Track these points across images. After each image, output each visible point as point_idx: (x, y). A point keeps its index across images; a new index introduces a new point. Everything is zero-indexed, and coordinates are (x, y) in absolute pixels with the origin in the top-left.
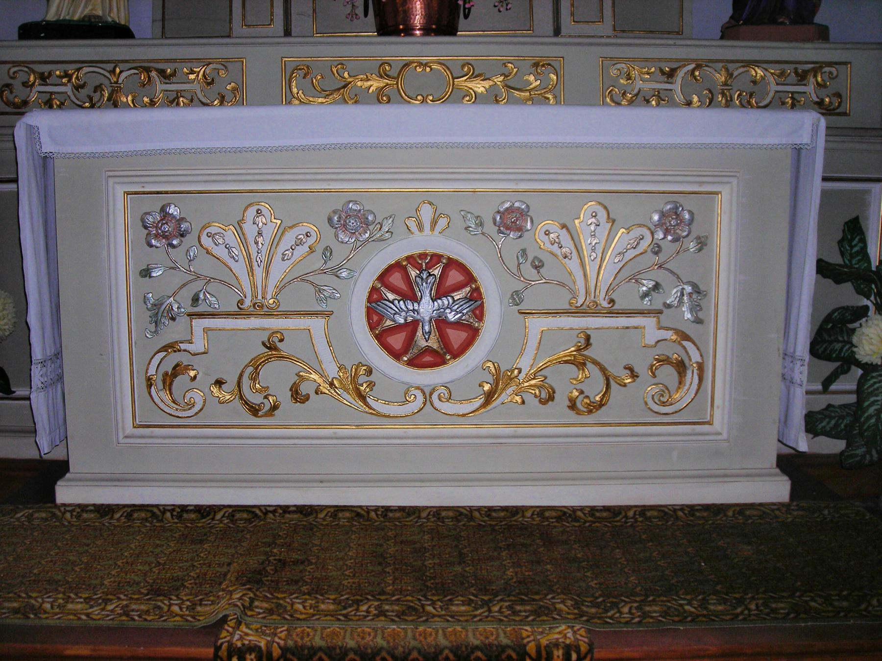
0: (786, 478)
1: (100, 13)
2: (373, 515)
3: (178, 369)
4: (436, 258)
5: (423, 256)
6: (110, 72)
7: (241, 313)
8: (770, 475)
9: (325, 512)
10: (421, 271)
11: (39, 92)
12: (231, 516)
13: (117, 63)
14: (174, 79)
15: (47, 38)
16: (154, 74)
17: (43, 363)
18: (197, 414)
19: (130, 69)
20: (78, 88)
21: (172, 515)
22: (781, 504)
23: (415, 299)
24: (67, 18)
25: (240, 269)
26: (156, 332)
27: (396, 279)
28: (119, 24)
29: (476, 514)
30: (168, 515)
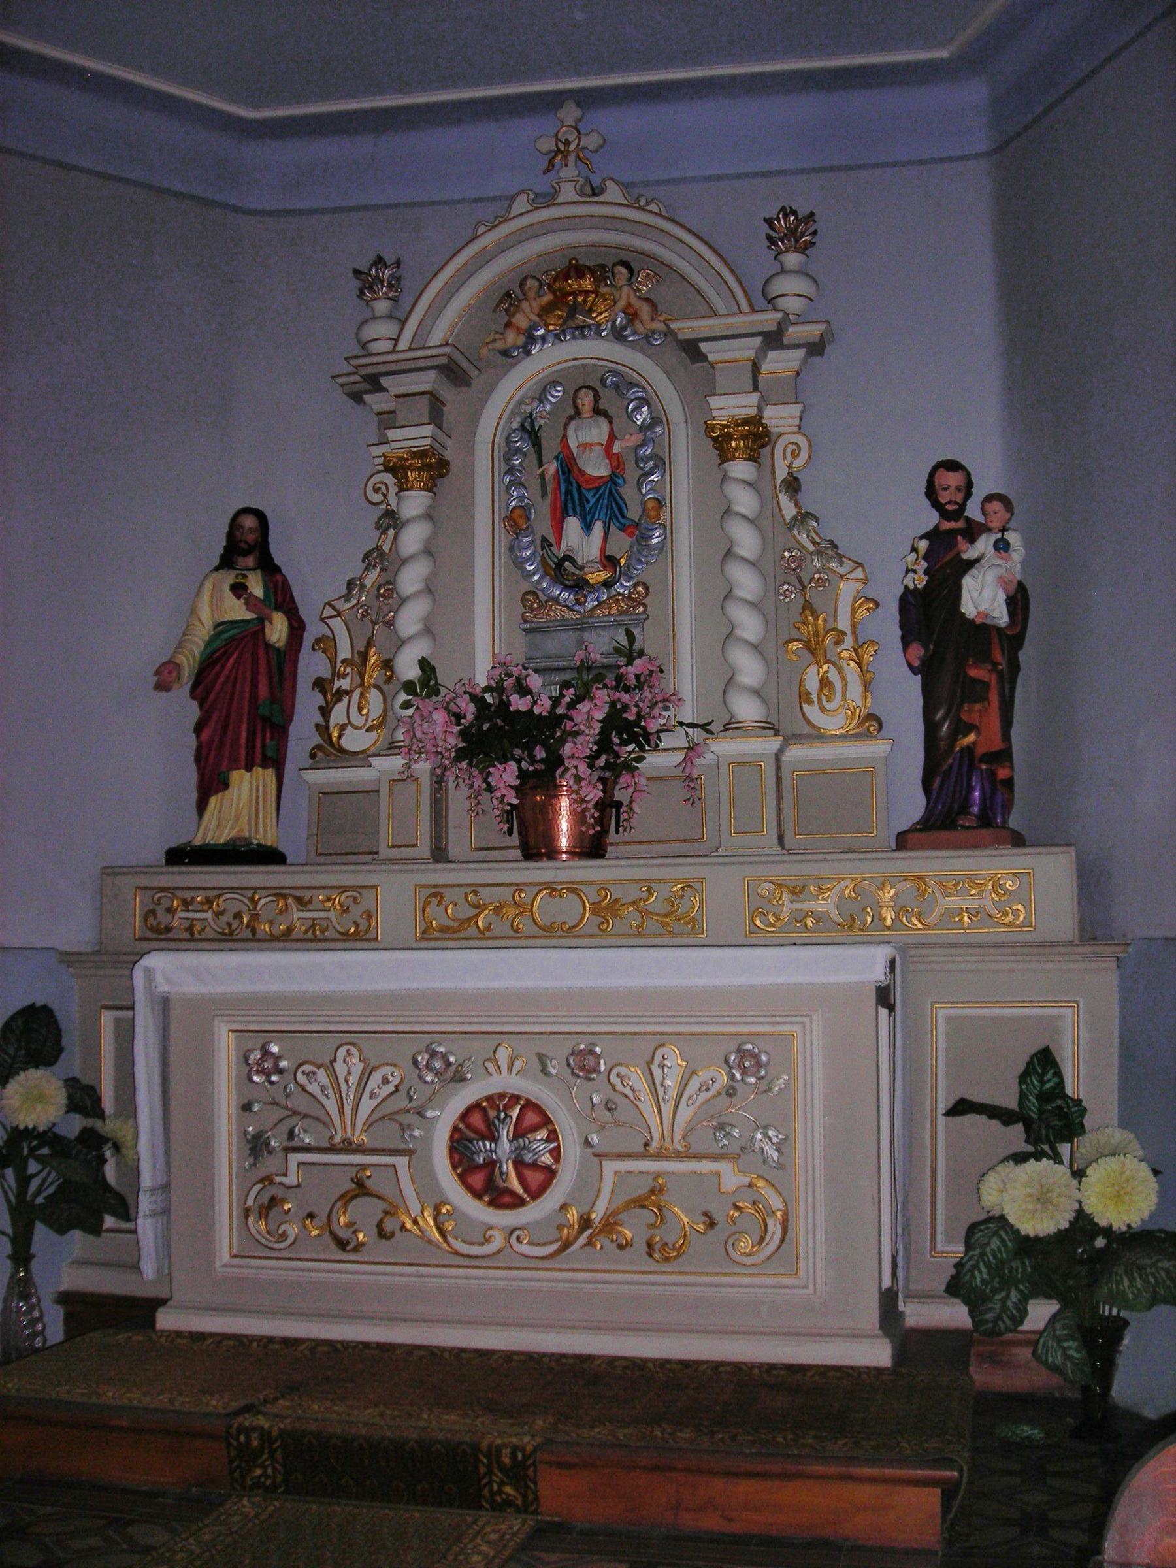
0: (887, 1340)
1: (247, 834)
2: (446, 1355)
3: (274, 1202)
4: (515, 1099)
5: (502, 1096)
6: (248, 898)
7: (332, 1149)
8: (872, 1337)
9: (813, 1371)
10: (499, 1111)
11: (181, 918)
12: (313, 1350)
13: (256, 889)
14: (310, 907)
15: (191, 863)
16: (290, 901)
17: (153, 1191)
18: (290, 1246)
19: (268, 896)
20: (218, 914)
21: (258, 1345)
22: (879, 1371)
23: (495, 1140)
24: (212, 842)
25: (331, 1105)
26: (255, 1165)
27: (531, 1118)
28: (265, 846)
29: (546, 1360)
30: (255, 1344)
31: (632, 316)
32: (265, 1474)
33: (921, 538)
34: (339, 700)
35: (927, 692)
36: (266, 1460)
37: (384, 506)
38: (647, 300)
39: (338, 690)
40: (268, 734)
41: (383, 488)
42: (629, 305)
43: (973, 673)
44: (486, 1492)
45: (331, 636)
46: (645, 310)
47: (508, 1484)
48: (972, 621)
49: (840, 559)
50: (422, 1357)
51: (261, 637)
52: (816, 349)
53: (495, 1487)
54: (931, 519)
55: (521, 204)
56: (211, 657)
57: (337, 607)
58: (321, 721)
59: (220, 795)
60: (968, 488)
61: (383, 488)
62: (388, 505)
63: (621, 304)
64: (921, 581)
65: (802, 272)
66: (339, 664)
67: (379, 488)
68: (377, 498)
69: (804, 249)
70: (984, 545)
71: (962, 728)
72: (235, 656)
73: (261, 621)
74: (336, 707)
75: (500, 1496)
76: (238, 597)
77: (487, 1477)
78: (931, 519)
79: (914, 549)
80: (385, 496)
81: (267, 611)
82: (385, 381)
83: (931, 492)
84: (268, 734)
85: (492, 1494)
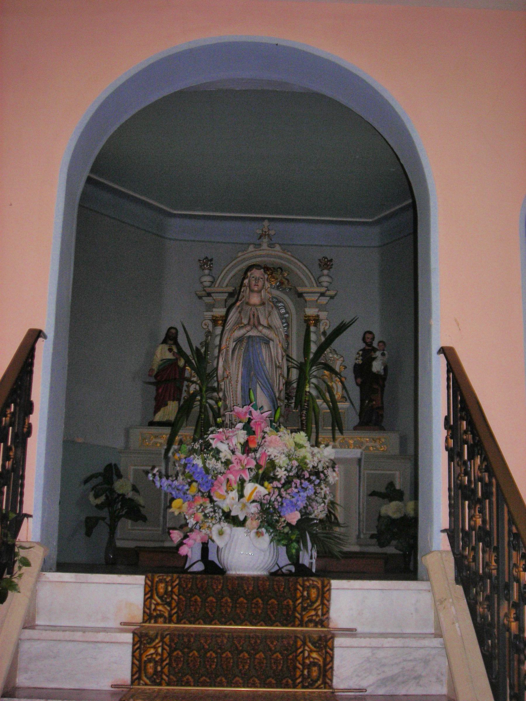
31: (282, 283)
32: (157, 653)
33: (360, 350)
35: (361, 392)
36: (158, 643)
38: (287, 279)
42: (281, 280)
43: (375, 387)
44: (300, 658)
46: (286, 282)
47: (314, 651)
48: (375, 373)
49: (337, 354)
50: (508, 629)
52: (332, 297)
53: (306, 654)
54: (362, 345)
55: (251, 248)
59: (165, 408)
60: (373, 339)
63: (279, 280)
64: (360, 362)
65: (328, 275)
68: (205, 327)
69: (329, 269)
70: (378, 354)
71: (371, 400)
73: (177, 360)
75: (309, 659)
76: (170, 352)
77: (302, 647)
78: (362, 345)
79: (358, 353)
80: (208, 327)
82: (212, 295)
83: (364, 339)
85: (304, 658)
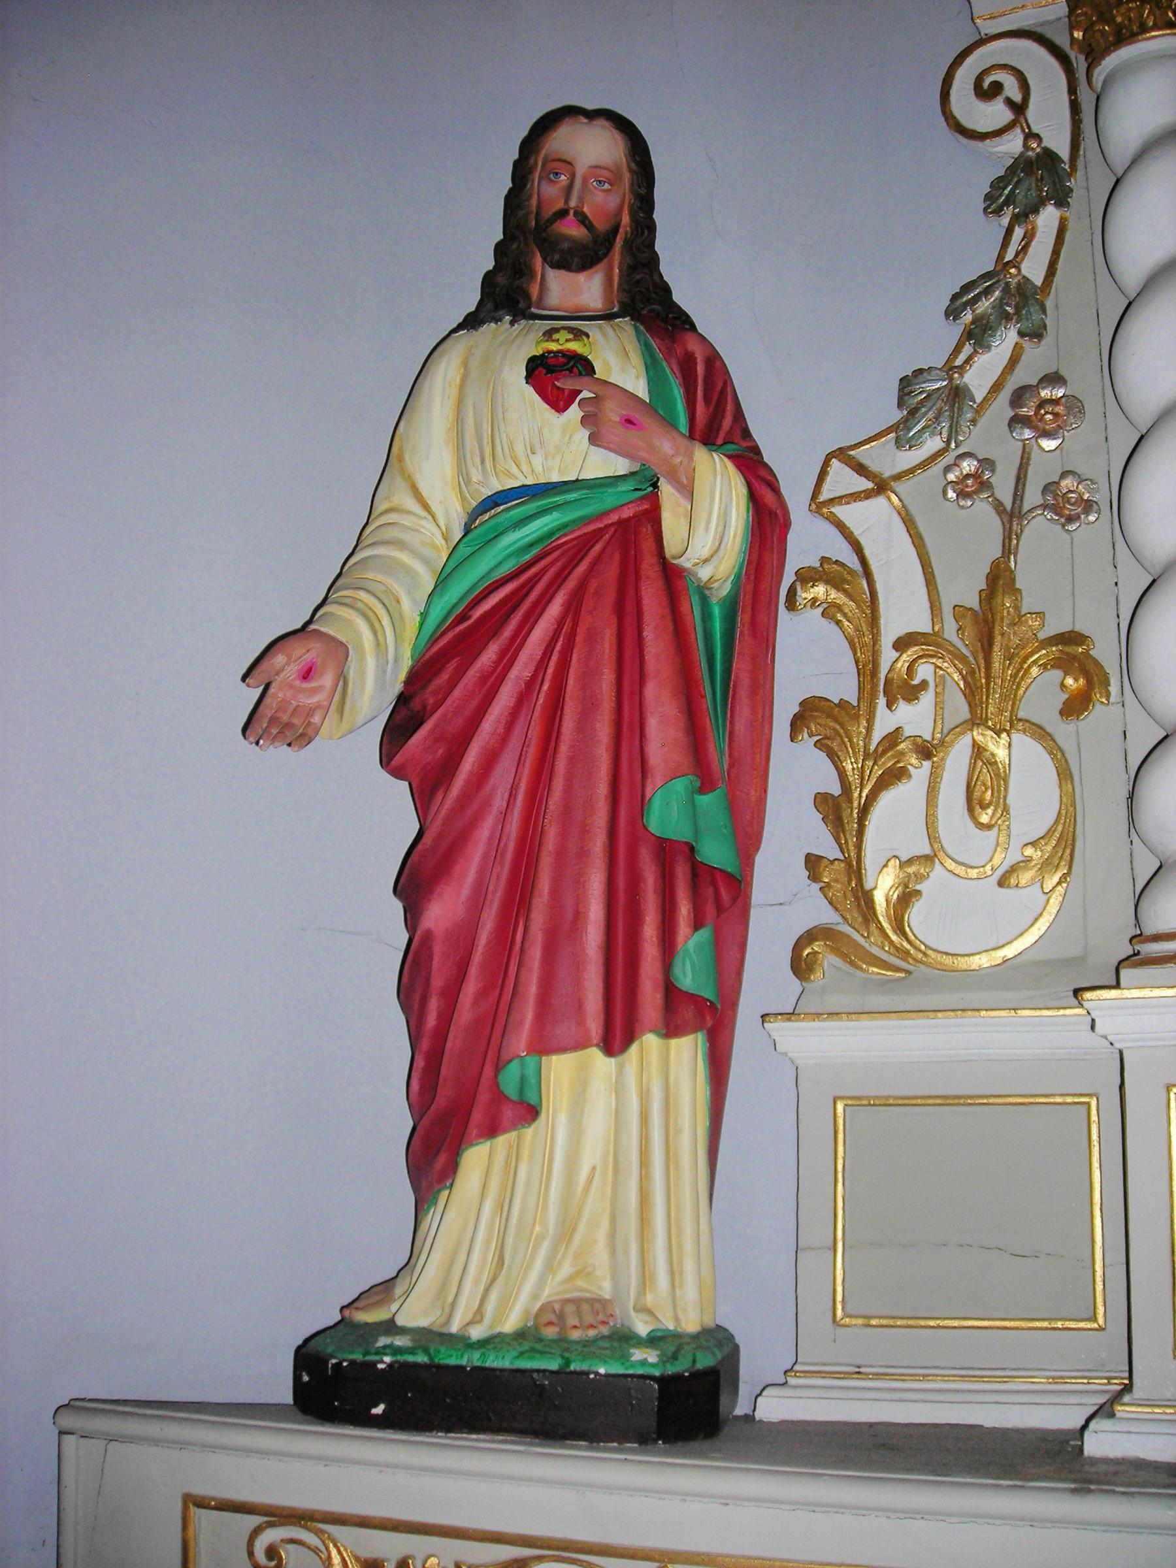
34: (896, 775)
37: (1013, 144)
39: (893, 738)
40: (684, 910)
41: (1012, 89)
45: (853, 562)
51: (648, 545)
56: (463, 617)
57: (873, 466)
58: (827, 847)
61: (1012, 89)
62: (1030, 135)
66: (888, 654)
67: (997, 88)
68: (995, 113)
72: (555, 608)
74: (887, 798)
76: (559, 402)
80: (1019, 109)
81: (666, 446)
84: (684, 910)
